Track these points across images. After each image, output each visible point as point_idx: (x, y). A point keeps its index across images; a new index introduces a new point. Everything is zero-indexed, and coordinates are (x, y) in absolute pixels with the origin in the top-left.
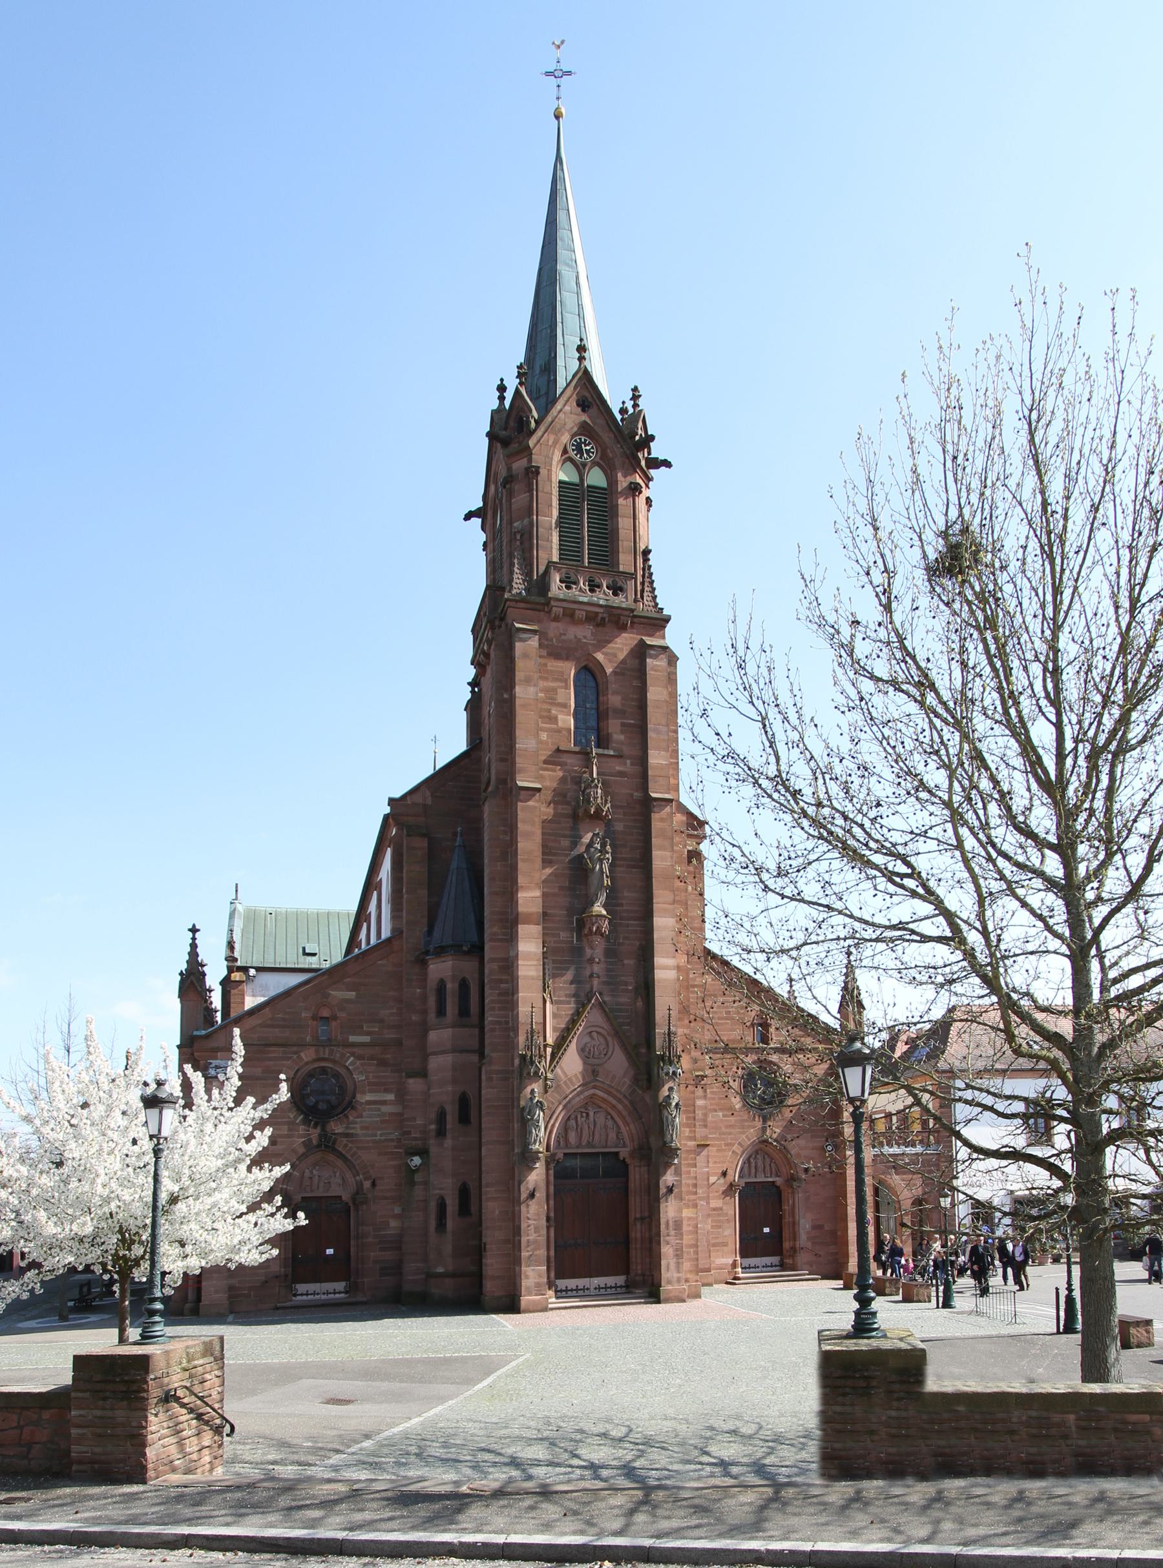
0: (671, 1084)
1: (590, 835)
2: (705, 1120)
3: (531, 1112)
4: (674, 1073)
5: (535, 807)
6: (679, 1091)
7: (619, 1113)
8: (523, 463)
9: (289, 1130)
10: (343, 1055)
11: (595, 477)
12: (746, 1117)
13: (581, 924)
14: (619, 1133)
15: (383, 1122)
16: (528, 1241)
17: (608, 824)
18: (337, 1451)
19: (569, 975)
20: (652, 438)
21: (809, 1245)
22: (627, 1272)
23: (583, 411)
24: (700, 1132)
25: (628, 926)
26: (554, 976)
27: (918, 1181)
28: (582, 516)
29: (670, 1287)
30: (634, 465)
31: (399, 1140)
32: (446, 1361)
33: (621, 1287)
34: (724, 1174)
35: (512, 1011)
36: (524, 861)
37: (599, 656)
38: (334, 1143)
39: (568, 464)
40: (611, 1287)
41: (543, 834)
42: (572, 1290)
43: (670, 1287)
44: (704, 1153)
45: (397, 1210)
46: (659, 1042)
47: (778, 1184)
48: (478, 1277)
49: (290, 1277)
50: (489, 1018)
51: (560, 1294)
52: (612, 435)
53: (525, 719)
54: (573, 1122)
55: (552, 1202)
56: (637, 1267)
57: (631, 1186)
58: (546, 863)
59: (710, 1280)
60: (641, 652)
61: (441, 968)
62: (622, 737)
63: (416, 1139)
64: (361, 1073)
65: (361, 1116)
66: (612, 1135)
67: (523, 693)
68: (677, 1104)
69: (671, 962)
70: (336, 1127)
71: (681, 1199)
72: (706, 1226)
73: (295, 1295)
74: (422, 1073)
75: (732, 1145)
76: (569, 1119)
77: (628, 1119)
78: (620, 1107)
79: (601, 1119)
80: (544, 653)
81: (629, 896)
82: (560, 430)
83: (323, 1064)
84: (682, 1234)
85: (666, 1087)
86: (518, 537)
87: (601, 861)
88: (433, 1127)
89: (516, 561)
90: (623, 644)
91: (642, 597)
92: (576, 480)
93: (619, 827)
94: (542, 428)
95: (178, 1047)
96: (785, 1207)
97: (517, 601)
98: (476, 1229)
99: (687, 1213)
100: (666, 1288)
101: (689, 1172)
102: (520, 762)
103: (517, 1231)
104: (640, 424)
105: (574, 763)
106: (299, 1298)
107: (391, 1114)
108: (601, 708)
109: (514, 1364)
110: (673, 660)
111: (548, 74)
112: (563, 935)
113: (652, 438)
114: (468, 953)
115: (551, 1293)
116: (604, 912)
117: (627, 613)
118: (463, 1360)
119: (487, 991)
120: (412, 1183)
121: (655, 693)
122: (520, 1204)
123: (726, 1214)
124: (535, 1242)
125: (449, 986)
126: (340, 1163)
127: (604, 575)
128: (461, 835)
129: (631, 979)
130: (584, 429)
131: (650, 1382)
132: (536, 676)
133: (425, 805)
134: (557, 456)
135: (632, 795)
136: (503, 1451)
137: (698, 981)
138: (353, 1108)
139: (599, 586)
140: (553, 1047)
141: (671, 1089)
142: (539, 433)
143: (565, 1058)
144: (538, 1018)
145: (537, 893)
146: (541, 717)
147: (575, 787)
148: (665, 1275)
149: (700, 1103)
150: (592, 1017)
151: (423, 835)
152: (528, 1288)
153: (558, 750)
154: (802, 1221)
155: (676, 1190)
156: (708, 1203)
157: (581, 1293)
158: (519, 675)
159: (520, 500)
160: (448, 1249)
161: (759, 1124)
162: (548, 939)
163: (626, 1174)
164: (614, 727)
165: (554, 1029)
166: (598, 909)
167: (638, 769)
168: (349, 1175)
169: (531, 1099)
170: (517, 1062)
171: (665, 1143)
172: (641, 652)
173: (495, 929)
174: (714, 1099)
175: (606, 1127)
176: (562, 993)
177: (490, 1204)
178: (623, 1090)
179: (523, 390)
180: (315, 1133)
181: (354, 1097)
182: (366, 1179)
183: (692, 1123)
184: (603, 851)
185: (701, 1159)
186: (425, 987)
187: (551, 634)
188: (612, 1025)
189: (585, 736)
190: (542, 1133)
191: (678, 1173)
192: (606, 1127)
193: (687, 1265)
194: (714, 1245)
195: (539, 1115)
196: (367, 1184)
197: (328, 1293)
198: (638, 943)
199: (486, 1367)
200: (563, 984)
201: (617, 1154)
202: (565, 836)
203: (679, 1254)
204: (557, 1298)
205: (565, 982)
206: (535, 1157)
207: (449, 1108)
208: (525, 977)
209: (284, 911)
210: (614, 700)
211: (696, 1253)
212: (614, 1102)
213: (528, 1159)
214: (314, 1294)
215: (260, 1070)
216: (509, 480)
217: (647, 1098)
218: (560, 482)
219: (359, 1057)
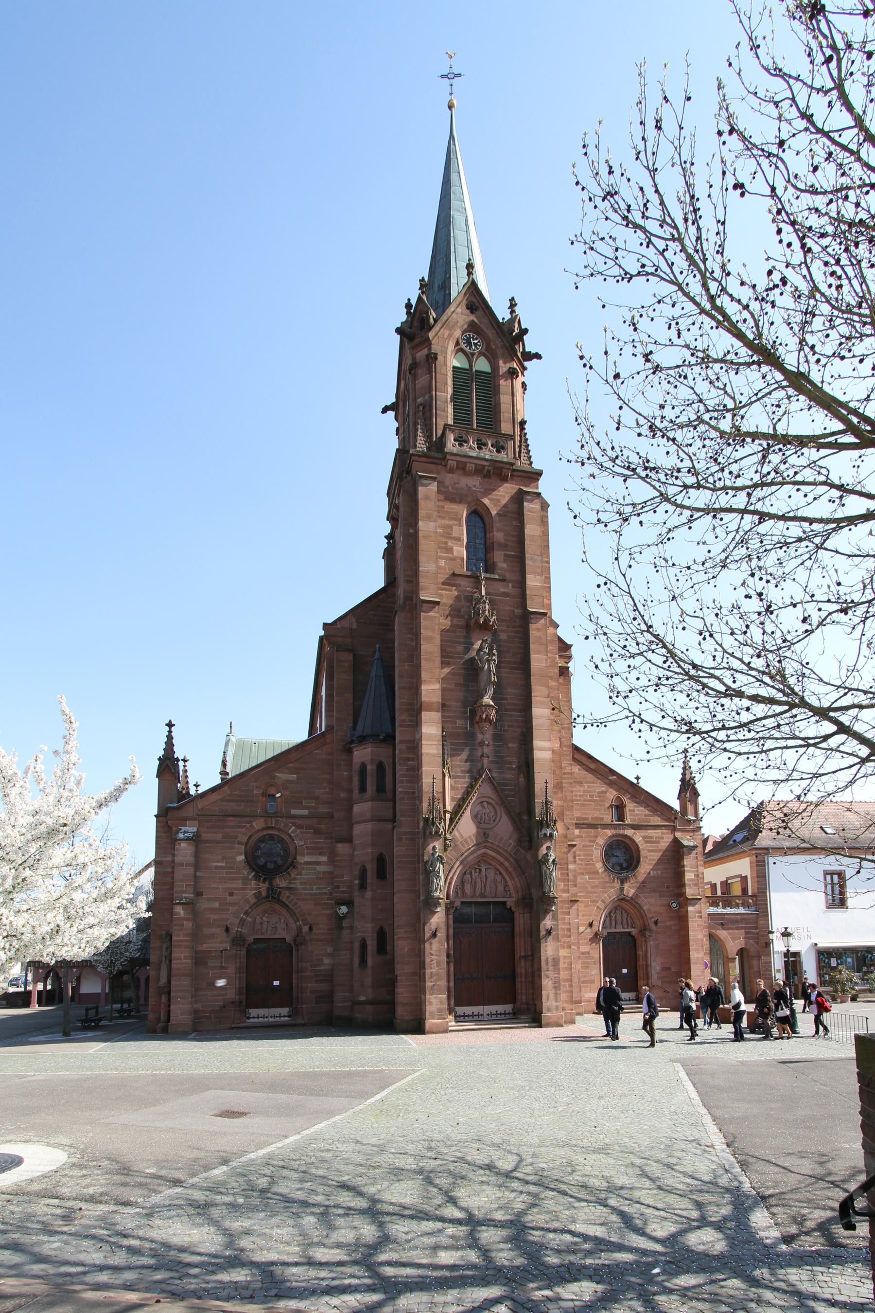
0: (548, 844)
1: (480, 642)
2: (575, 881)
3: (433, 865)
4: (551, 835)
5: (435, 617)
6: (555, 851)
7: (506, 869)
8: (425, 351)
9: (243, 884)
10: (286, 825)
11: (482, 365)
12: (607, 879)
13: (473, 713)
14: (506, 886)
15: (317, 878)
16: (431, 973)
17: (495, 633)
18: (176, 1182)
19: (464, 755)
20: (526, 331)
21: (659, 983)
22: (513, 1001)
23: (472, 312)
24: (573, 890)
25: (511, 716)
26: (452, 755)
27: (741, 933)
28: (471, 394)
29: (550, 1014)
30: (511, 354)
31: (331, 894)
32: (350, 1074)
33: (509, 1014)
34: (591, 925)
35: (418, 783)
36: (426, 660)
37: (486, 501)
38: (279, 895)
39: (460, 354)
40: (501, 1014)
41: (442, 640)
42: (469, 1016)
43: (550, 1014)
44: (575, 907)
45: (330, 950)
46: (538, 810)
47: (633, 934)
48: (391, 1004)
49: (244, 1002)
51: (459, 1018)
52: (494, 332)
53: (426, 548)
54: (468, 877)
55: (451, 942)
56: (522, 998)
57: (517, 930)
58: (444, 664)
59: (581, 1010)
60: (519, 498)
61: (363, 754)
62: (505, 565)
63: (344, 892)
64: (301, 839)
65: (300, 874)
66: (501, 888)
67: (425, 527)
68: (554, 861)
69: (546, 744)
70: (281, 882)
71: (558, 940)
72: (578, 966)
73: (248, 1018)
74: (349, 839)
75: (597, 902)
76: (465, 873)
77: (514, 874)
78: (507, 864)
79: (491, 875)
80: (442, 497)
81: (512, 692)
82: (453, 327)
83: (271, 832)
84: (559, 970)
85: (544, 847)
86: (421, 409)
87: (489, 661)
88: (357, 882)
89: (419, 427)
90: (505, 492)
91: (520, 457)
92: (467, 366)
93: (503, 636)
94: (439, 324)
96: (640, 953)
97: (420, 456)
98: (388, 967)
99: (563, 953)
100: (546, 1015)
101: (564, 919)
102: (422, 581)
103: (422, 965)
104: (516, 325)
105: (467, 585)
106: (252, 1020)
107: (324, 873)
108: (488, 543)
109: (409, 1078)
110: (545, 506)
111: (443, 76)
112: (459, 722)
113: (526, 331)
114: (384, 741)
115: (451, 1017)
116: (492, 703)
117: (507, 466)
118: (364, 1074)
119: (398, 767)
120: (340, 928)
121: (531, 530)
122: (424, 942)
123: (593, 958)
124: (437, 974)
125: (369, 767)
126: (284, 911)
127: (489, 437)
128: (379, 651)
129: (514, 760)
130: (472, 327)
131: (537, 1100)
132: (435, 514)
133: (351, 629)
134: (451, 347)
135: (513, 611)
136: (365, 1190)
137: (568, 770)
138: (294, 867)
139: (485, 445)
140: (451, 813)
141: (548, 848)
142: (436, 328)
143: (461, 822)
144: (438, 788)
145: (437, 686)
146: (439, 548)
147: (468, 604)
148: (546, 1004)
149: (571, 866)
150: (483, 789)
151: (350, 651)
152: (431, 1013)
153: (454, 574)
154: (653, 964)
155: (553, 933)
156: (578, 948)
157: (476, 1018)
158: (422, 513)
159: (422, 381)
160: (368, 981)
161: (617, 885)
162: (446, 725)
163: (512, 920)
164: (498, 557)
165: (452, 799)
166: (487, 700)
167: (516, 591)
168: (291, 921)
169: (433, 854)
170: (421, 824)
171: (544, 893)
172: (519, 498)
173: (404, 717)
174: (581, 864)
175: (495, 881)
176: (459, 770)
177: (400, 942)
179: (424, 297)
180: (264, 887)
181: (295, 858)
182: (305, 924)
183: (565, 878)
184: (490, 654)
185: (573, 910)
186: (350, 770)
187: (447, 483)
188: (499, 796)
189: (475, 565)
190: (442, 883)
191: (555, 918)
192: (495, 881)
193: (563, 996)
194: (584, 982)
195: (439, 867)
196: (305, 929)
197: (275, 1017)
198: (519, 730)
199: (383, 1080)
200: (459, 762)
201: (504, 903)
202: (459, 643)
203: (557, 986)
204: (456, 1022)
205: (461, 761)
206: (436, 902)
207: (369, 867)
208: (428, 754)
209: (264, 741)
210: (498, 536)
211: (571, 986)
212: (502, 860)
213: (431, 904)
214: (263, 1017)
215: (220, 835)
216: (414, 366)
217: (529, 857)
218: (454, 367)
219: (300, 827)
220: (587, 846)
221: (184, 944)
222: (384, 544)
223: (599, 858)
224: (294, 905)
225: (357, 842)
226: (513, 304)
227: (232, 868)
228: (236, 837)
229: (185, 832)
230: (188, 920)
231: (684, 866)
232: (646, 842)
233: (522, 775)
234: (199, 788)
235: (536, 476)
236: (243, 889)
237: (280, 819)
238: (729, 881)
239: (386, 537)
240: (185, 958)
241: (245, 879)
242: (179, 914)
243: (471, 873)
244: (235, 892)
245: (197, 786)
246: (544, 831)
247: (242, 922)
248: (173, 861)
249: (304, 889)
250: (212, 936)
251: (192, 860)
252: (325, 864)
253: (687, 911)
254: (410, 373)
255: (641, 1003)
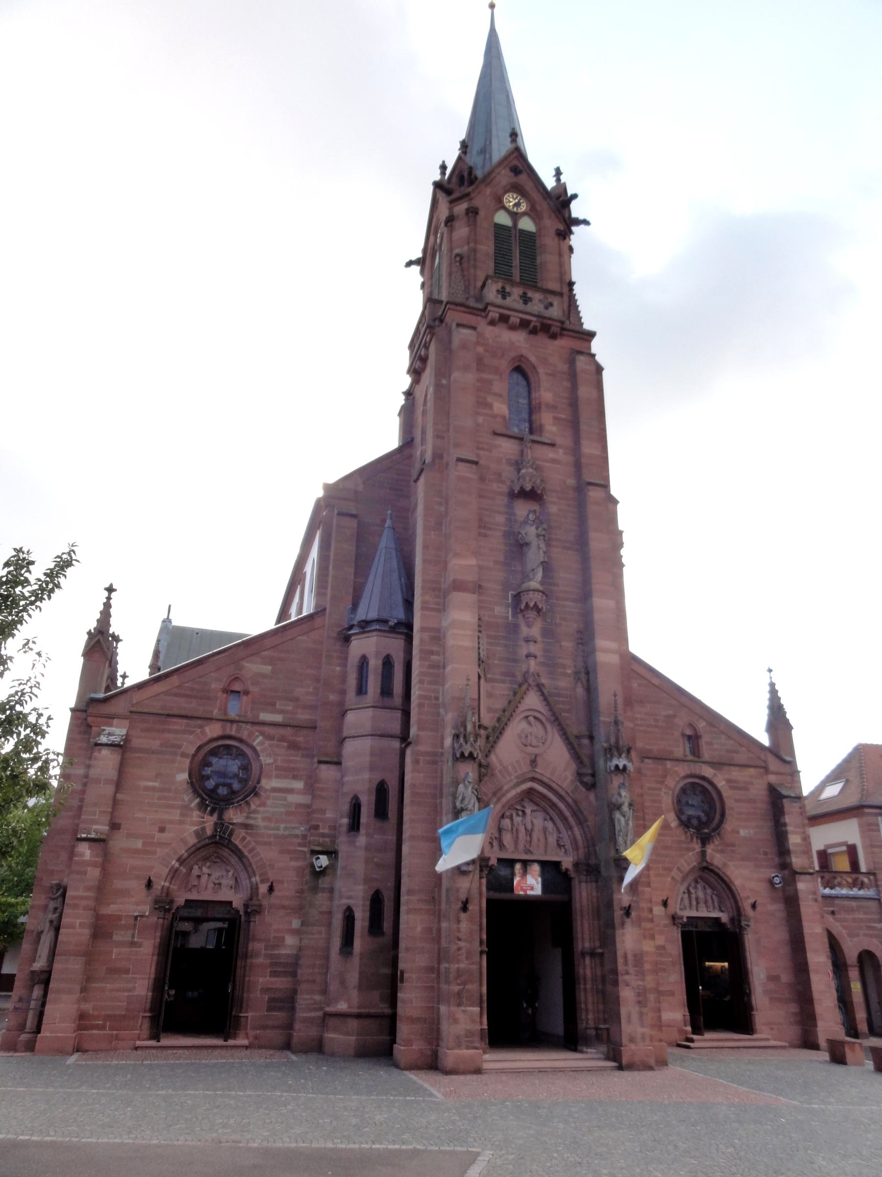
9: (182, 815)
10: (251, 734)
12: (683, 838)
15: (288, 813)
29: (633, 1047)
31: (304, 837)
38: (231, 834)
50: (416, 692)
62: (554, 429)
63: (323, 835)
65: (263, 804)
70: (234, 816)
75: (669, 870)
86: (458, 259)
88: (345, 821)
95: (72, 710)
107: (298, 806)
108: (534, 403)
112: (499, 610)
114: (393, 630)
126: (234, 860)
129: (569, 662)
160: (353, 977)
161: (697, 847)
178: (565, 785)
180: (210, 821)
181: (258, 782)
182: (263, 881)
186: (344, 665)
196: (263, 888)
215: (158, 742)
219: (270, 738)
220: (654, 789)
221: (84, 903)
222: (401, 400)
223: (671, 806)
224: (251, 851)
225: (347, 763)
226: (558, 173)
227: (169, 791)
228: (180, 747)
229: (109, 734)
230: (95, 865)
231: (785, 825)
232: (731, 788)
233: (579, 685)
234: (126, 680)
235: (589, 338)
236: (181, 822)
237: (244, 725)
238: (830, 851)
239: (404, 393)
240: (82, 925)
241: (186, 808)
242: (82, 855)
243: (511, 818)
244: (168, 826)
245: (124, 676)
246: (615, 762)
247: (174, 873)
248: (86, 776)
249: (267, 828)
250: (125, 893)
251: (113, 774)
252: (299, 792)
253: (796, 890)
254: (446, 225)
255: (267, 1011)
